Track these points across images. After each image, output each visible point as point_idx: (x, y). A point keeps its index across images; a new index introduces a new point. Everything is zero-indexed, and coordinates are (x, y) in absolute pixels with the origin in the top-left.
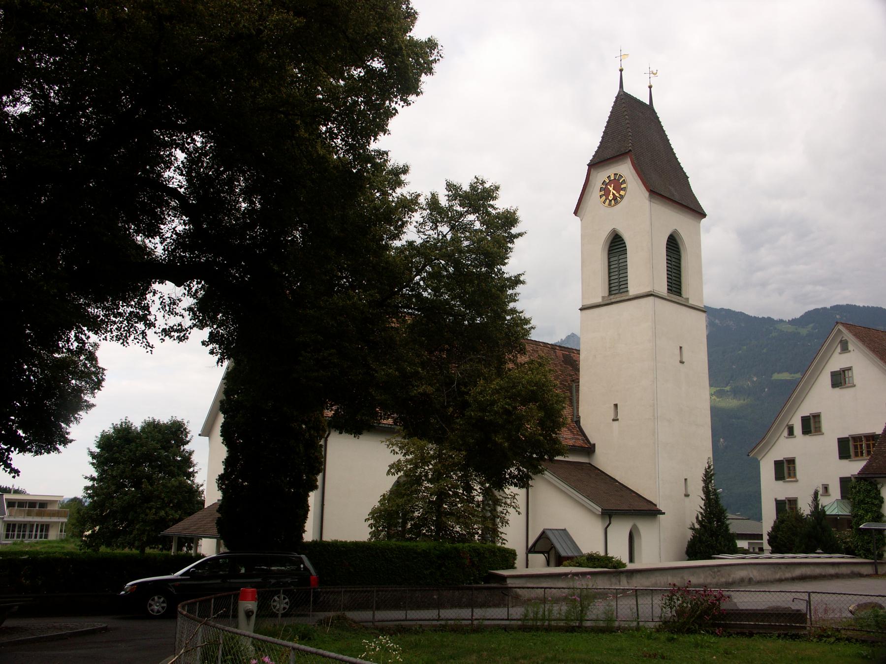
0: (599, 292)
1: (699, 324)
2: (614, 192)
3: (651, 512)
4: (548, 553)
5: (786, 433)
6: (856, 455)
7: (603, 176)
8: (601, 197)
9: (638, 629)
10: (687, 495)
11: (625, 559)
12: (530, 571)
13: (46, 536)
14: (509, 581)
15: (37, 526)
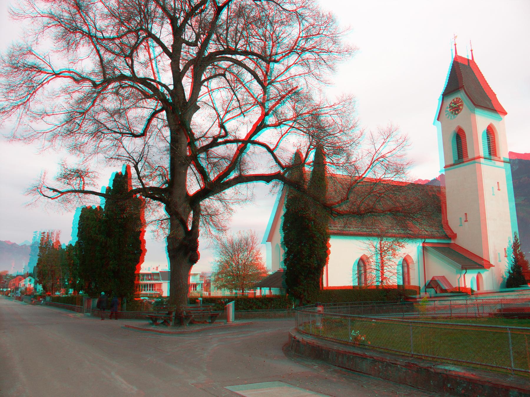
2: (456, 109)
4: (436, 287)
7: (450, 100)
11: (475, 288)
13: (196, 289)
15: (150, 285)
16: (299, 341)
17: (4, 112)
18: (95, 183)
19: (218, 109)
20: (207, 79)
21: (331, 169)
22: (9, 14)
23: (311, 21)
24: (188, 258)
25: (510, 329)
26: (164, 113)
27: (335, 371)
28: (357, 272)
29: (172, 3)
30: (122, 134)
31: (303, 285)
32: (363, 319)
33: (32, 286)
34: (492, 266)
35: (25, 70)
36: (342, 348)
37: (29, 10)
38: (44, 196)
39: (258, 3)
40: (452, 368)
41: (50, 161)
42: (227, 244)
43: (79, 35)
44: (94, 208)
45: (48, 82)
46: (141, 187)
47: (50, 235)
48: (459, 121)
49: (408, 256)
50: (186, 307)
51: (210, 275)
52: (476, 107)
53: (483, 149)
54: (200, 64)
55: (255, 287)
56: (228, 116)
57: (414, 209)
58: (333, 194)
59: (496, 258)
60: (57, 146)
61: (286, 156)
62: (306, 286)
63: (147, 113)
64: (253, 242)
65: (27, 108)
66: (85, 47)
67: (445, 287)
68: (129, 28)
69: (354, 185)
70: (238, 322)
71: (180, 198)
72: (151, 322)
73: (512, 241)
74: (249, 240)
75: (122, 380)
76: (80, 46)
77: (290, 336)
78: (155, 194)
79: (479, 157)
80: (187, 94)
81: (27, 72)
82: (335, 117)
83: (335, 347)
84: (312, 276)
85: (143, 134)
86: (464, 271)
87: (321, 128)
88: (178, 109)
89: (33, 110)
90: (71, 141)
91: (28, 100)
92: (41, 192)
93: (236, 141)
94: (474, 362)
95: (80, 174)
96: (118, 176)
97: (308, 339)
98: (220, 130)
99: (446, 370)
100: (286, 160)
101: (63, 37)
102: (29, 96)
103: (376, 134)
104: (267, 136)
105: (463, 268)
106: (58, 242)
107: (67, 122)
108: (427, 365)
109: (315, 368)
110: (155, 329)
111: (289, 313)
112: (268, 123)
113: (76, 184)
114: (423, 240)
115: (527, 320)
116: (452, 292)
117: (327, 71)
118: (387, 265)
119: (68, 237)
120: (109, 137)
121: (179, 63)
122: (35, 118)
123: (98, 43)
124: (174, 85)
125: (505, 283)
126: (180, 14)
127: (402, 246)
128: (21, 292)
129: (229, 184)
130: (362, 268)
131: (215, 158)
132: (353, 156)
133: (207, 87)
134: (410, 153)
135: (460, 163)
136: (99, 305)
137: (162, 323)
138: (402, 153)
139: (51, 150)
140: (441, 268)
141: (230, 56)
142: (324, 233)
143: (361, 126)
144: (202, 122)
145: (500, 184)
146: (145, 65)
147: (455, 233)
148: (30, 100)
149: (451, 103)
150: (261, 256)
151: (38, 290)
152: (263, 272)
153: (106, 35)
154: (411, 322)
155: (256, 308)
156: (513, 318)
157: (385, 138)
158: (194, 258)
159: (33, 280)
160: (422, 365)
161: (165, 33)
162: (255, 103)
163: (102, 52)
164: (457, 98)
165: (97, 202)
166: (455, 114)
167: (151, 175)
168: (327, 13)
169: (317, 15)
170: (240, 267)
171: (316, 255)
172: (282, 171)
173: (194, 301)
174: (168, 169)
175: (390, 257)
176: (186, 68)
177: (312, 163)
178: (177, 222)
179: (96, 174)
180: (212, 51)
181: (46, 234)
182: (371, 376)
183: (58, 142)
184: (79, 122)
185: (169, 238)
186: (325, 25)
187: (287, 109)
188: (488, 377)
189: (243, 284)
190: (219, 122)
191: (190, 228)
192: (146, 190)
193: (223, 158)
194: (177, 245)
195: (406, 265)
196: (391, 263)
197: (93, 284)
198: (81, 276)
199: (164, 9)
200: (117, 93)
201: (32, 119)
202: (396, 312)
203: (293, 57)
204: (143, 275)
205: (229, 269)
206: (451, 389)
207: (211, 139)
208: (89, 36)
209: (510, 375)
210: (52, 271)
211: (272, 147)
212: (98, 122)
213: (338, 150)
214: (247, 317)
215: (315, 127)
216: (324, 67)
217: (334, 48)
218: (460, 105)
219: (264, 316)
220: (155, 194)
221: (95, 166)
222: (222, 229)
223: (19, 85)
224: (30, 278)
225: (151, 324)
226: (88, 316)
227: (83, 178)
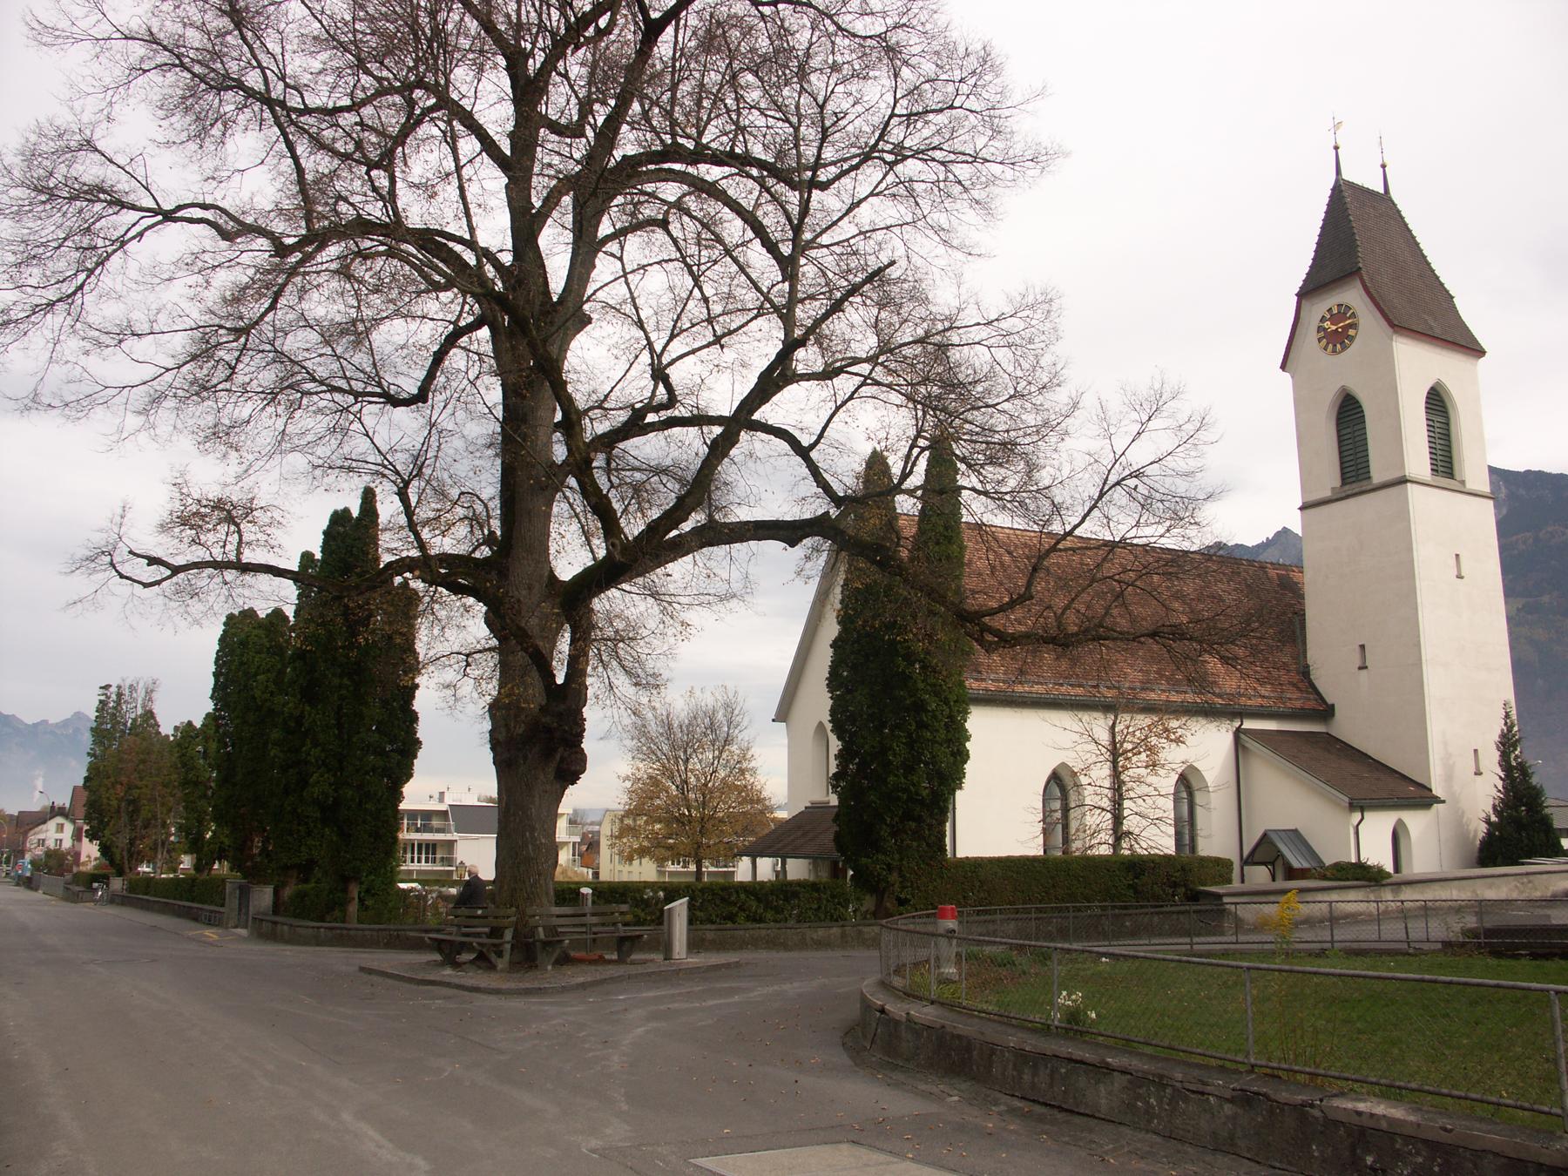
0: (1330, 478)
1: (1483, 517)
2: (1338, 336)
3: (1422, 798)
4: (1273, 864)
8: (1320, 340)
9: (219, 91)
10: (1478, 773)
11: (1389, 867)
12: (1246, 887)
14: (1226, 900)
15: (420, 846)
16: (897, 1023)
17: (6, 324)
18: (272, 542)
19: (646, 325)
20: (620, 234)
21: (975, 509)
22: (25, 29)
23: (928, 68)
24: (551, 770)
25: (1557, 992)
26: (484, 333)
27: (1012, 1111)
28: (1041, 816)
29: (513, 6)
30: (357, 395)
31: (885, 853)
32: (1074, 955)
33: (67, 844)
34: (1438, 800)
35: (72, 199)
36: (1032, 1043)
37: (88, 22)
38: (122, 576)
39: (767, 10)
40: (1380, 1109)
41: (139, 474)
42: (654, 728)
43: (231, 99)
44: (262, 615)
45: (141, 234)
46: (415, 553)
47: (127, 692)
48: (1345, 371)
49: (1191, 767)
50: (546, 914)
51: (597, 819)
52: (1395, 332)
53: (1417, 460)
54: (595, 186)
55: (735, 854)
56: (677, 348)
57: (1215, 629)
58: (980, 582)
59: (1449, 778)
60: (164, 429)
61: (845, 471)
62: (897, 856)
63: (429, 334)
64: (730, 723)
65: (75, 310)
66: (249, 133)
67: (1297, 862)
68: (379, 80)
69: (1044, 555)
70: (696, 960)
71: (530, 588)
72: (438, 957)
73: (1498, 727)
74: (720, 716)
75: (378, 1137)
76: (237, 129)
77: (866, 1006)
78: (455, 574)
79: (1403, 481)
80: (557, 283)
81: (80, 206)
82: (1003, 355)
83: (1013, 1040)
84: (913, 825)
85: (421, 396)
86: (1357, 816)
87: (951, 384)
88: (527, 324)
89: (91, 319)
90: (202, 414)
91: (81, 287)
92: (112, 565)
93: (700, 420)
94: (1445, 1091)
95: (229, 513)
96: (340, 518)
97: (924, 1013)
98: (656, 387)
99: (1359, 1113)
100: (845, 479)
101: (185, 103)
102: (82, 277)
103: (1115, 405)
104: (793, 407)
105: (1353, 807)
106: (149, 715)
107: (194, 358)
108: (1300, 1098)
109: (950, 1101)
110: (456, 981)
111: (843, 935)
112: (801, 369)
113: (218, 542)
114: (1237, 724)
115: (1553, 965)
116: (1324, 878)
117: (971, 215)
118: (1132, 794)
119: (184, 696)
120: (322, 404)
121: (529, 188)
122: (99, 344)
123: (292, 122)
124: (516, 251)
125: (1476, 854)
126: (534, 44)
127: (1178, 741)
128: (32, 862)
129: (680, 548)
130: (1057, 805)
131: (638, 470)
132: (1044, 473)
133: (621, 259)
134: (1215, 462)
135: (1347, 497)
136: (277, 907)
137: (472, 962)
138: (1193, 464)
139: (143, 437)
140: (1291, 803)
141: (677, 167)
142: (953, 697)
143: (1074, 381)
144: (598, 363)
145: (1462, 559)
146: (428, 190)
147: (1330, 701)
148: (86, 288)
149: (1323, 319)
150: (753, 764)
151: (83, 858)
152: (762, 812)
153: (313, 101)
154: (1249, 968)
155: (748, 918)
156: (1516, 957)
157: (1145, 418)
158: (571, 767)
159: (69, 828)
160: (1284, 1096)
161: (490, 97)
162: (761, 307)
163: (302, 149)
164: (1340, 306)
165: (281, 597)
166: (1334, 351)
167: (437, 519)
168: (979, 46)
169: (945, 54)
170: (692, 796)
171: (926, 764)
172: (834, 513)
173: (568, 894)
174: (491, 505)
175: (1143, 771)
176: (551, 201)
177: (919, 493)
178: (521, 658)
179: (277, 514)
180: (631, 150)
181: (114, 689)
182: (1122, 1128)
183: (165, 415)
184: (227, 358)
185: (494, 708)
186: (972, 81)
187: (855, 329)
188: (1492, 1136)
189: (699, 845)
190: (652, 364)
191: (560, 680)
192: (432, 563)
193: (660, 471)
194: (520, 730)
195: (1184, 795)
196: (1143, 789)
197: (258, 842)
198: (218, 818)
199: (488, 26)
200: (344, 272)
201: (88, 346)
202: (1160, 935)
203: (871, 174)
204: (413, 814)
205: (658, 802)
206: (1375, 1170)
207: (622, 417)
208: (266, 100)
209: (1559, 1133)
210: (130, 802)
211: (806, 441)
212: (280, 356)
213: (1002, 452)
214: (719, 946)
215: (934, 380)
216: (962, 205)
217: (992, 150)
218: (1351, 326)
219: (772, 944)
220: (455, 574)
221: (275, 489)
222: (648, 682)
223: (55, 244)
224: (60, 820)
225: (442, 964)
226: (241, 939)
227: (237, 525)
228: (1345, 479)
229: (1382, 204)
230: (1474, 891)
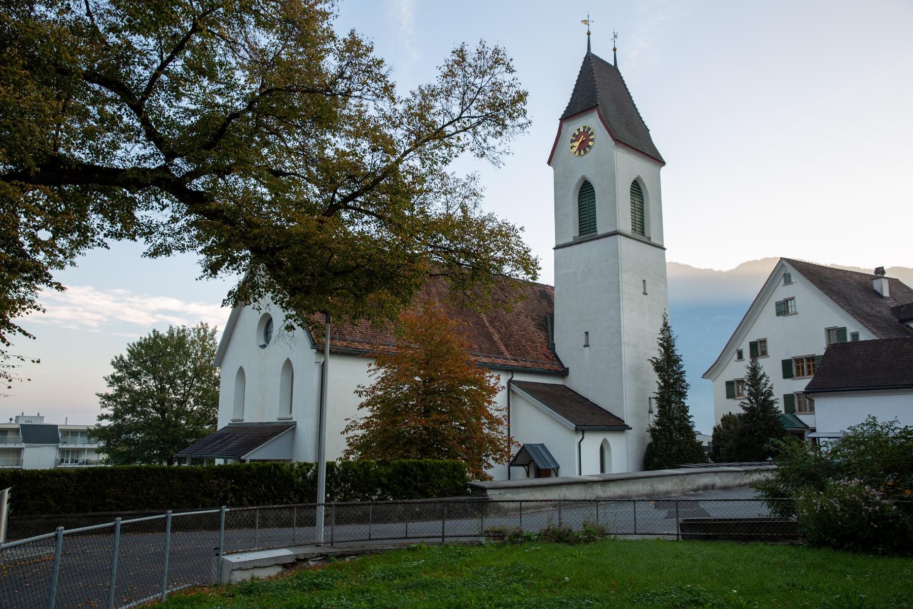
0: (572, 231)
3: (617, 425)
4: (528, 465)
5: (736, 356)
6: (798, 375)
53: (625, 223)
105: (577, 430)
228: (581, 232)
229: (613, 71)
230: (652, 486)
